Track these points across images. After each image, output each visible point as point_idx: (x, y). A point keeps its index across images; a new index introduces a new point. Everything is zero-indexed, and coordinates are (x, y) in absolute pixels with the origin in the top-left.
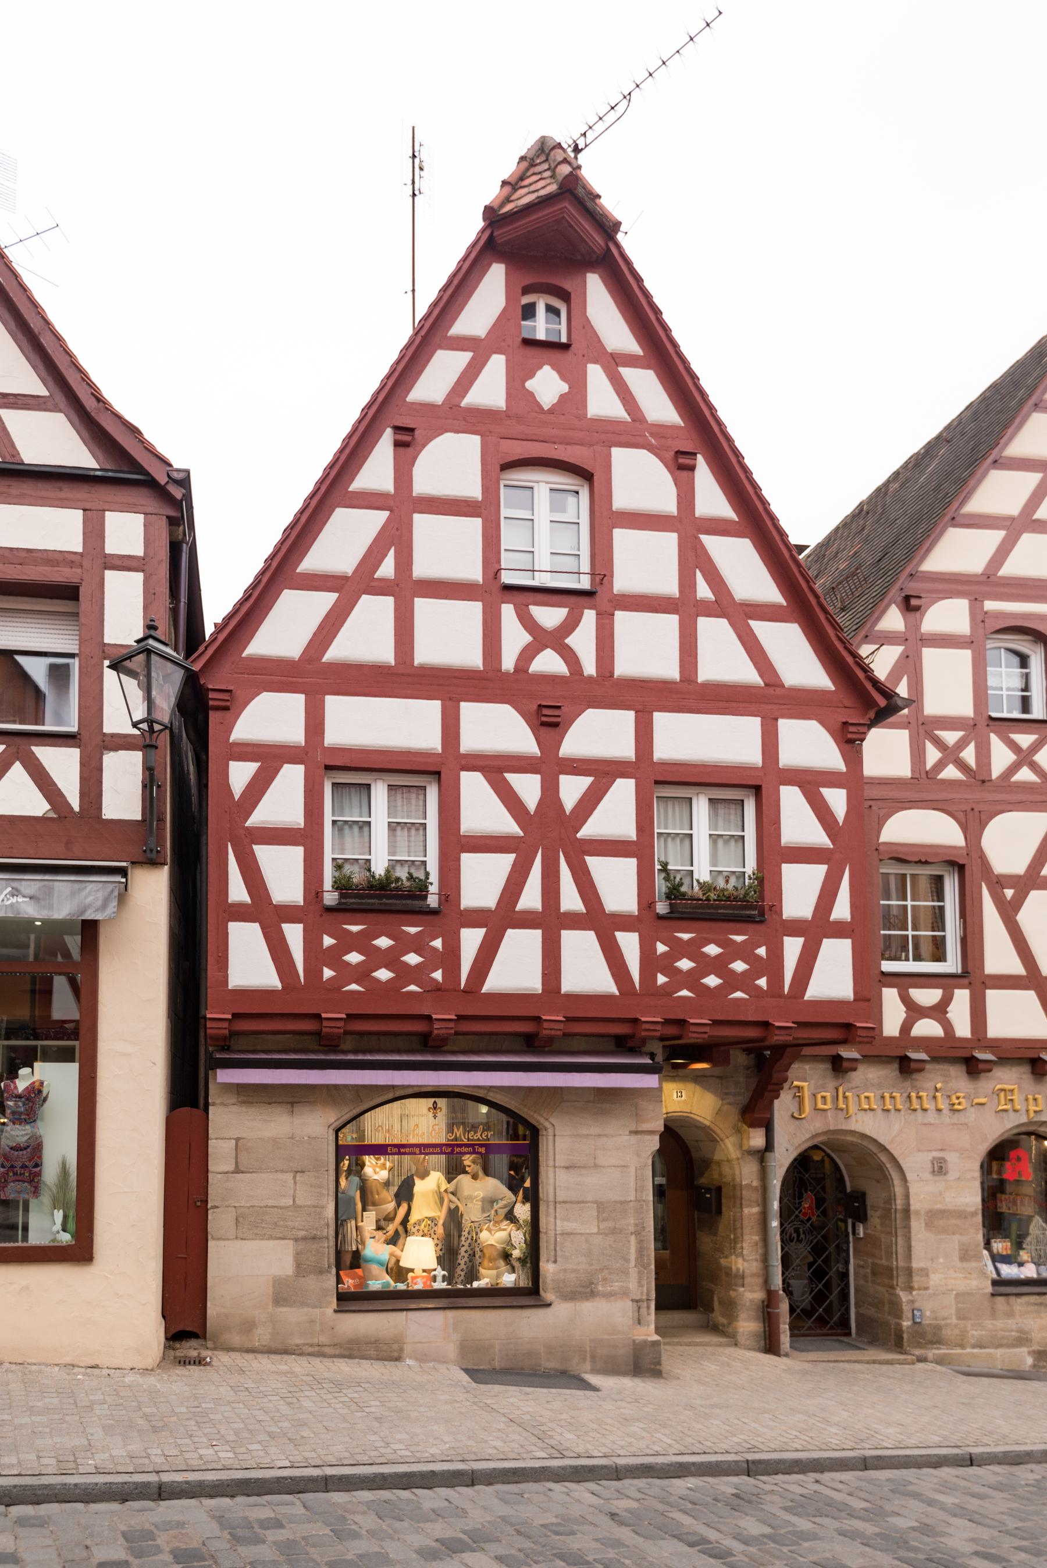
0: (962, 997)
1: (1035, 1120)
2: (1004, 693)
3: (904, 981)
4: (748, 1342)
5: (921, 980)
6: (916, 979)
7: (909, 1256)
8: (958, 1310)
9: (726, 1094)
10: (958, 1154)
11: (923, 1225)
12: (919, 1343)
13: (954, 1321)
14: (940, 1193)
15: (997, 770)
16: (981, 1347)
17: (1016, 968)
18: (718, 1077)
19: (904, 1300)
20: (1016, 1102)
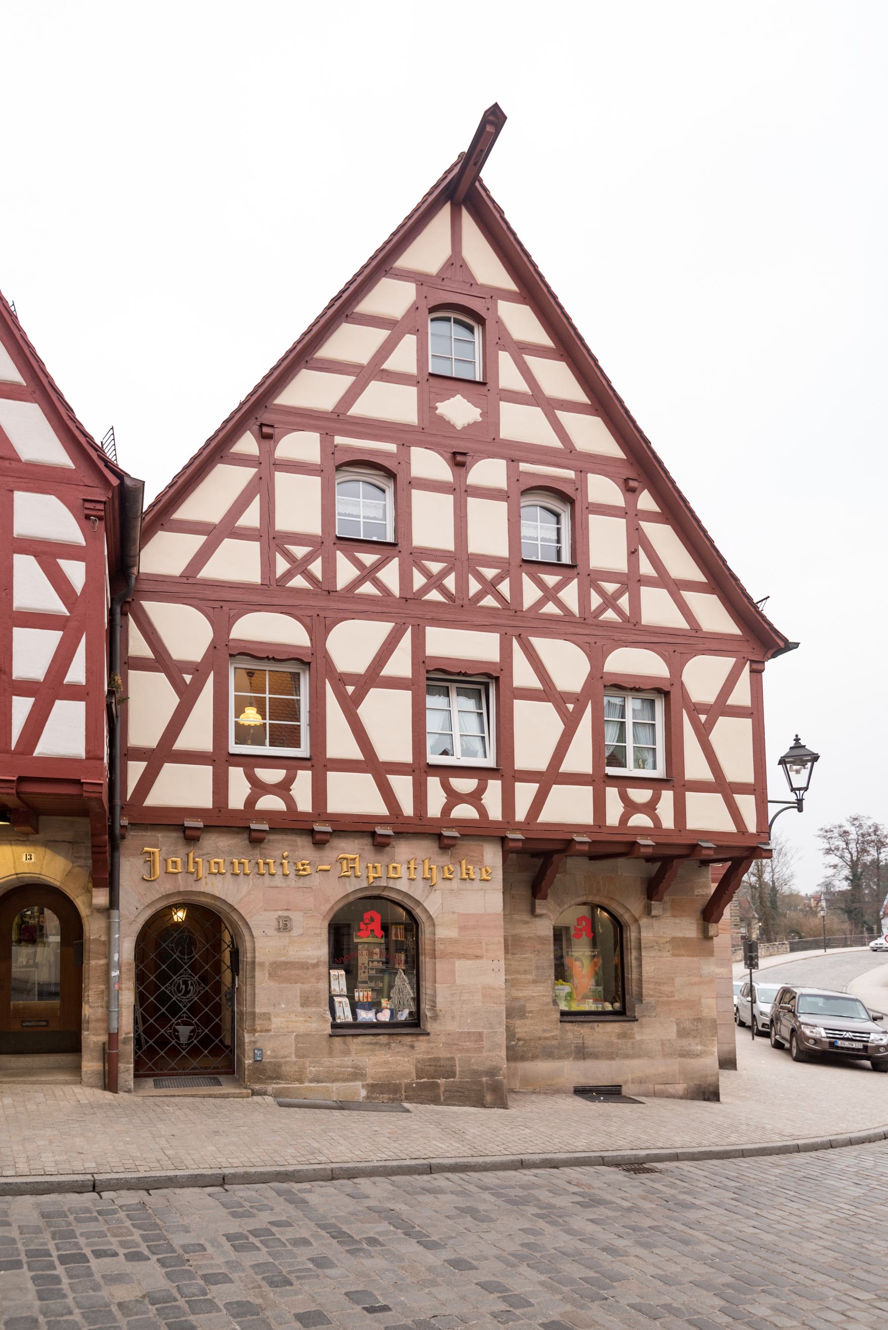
0: (667, 796)
1: (374, 885)
2: (362, 520)
3: (249, 762)
4: (91, 1080)
5: (268, 761)
6: (261, 760)
7: (253, 1004)
8: (297, 1049)
9: (77, 857)
10: (302, 914)
11: (267, 975)
12: (259, 1079)
13: (294, 1059)
14: (284, 948)
15: (342, 582)
16: (318, 1082)
17: (355, 753)
18: (69, 842)
19: (246, 1041)
20: (357, 869)
